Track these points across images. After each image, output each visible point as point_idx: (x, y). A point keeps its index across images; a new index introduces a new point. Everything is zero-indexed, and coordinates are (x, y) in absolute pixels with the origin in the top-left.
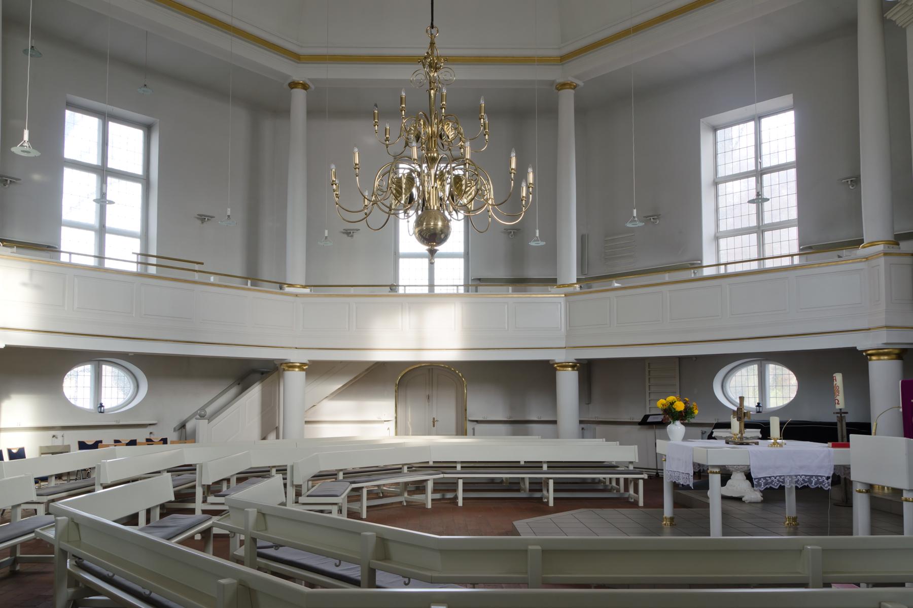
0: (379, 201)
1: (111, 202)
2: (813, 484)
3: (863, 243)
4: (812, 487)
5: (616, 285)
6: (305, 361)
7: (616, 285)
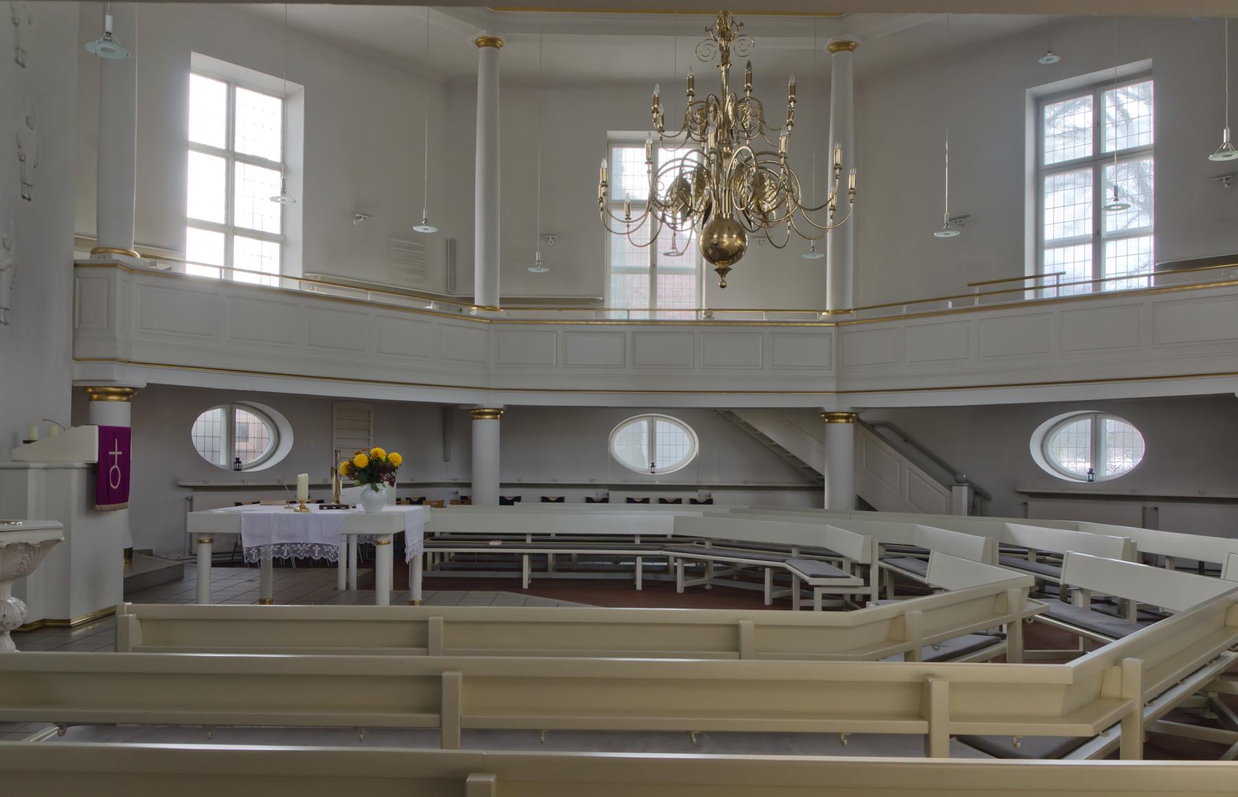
1: (273, 199)
2: (286, 554)
4: (316, 559)
6: (501, 406)
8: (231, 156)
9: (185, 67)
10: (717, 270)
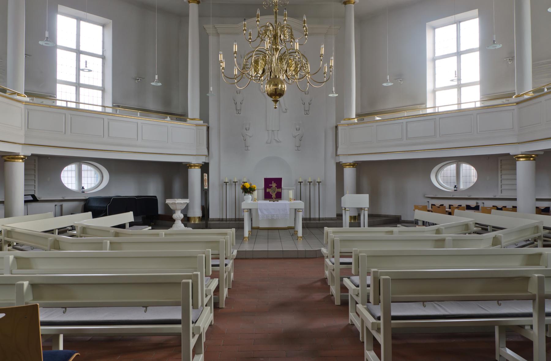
0: (306, 72)
3: (515, 94)
5: (378, 118)
7: (378, 118)
8: (78, 52)
9: (55, 11)
10: (273, 101)
